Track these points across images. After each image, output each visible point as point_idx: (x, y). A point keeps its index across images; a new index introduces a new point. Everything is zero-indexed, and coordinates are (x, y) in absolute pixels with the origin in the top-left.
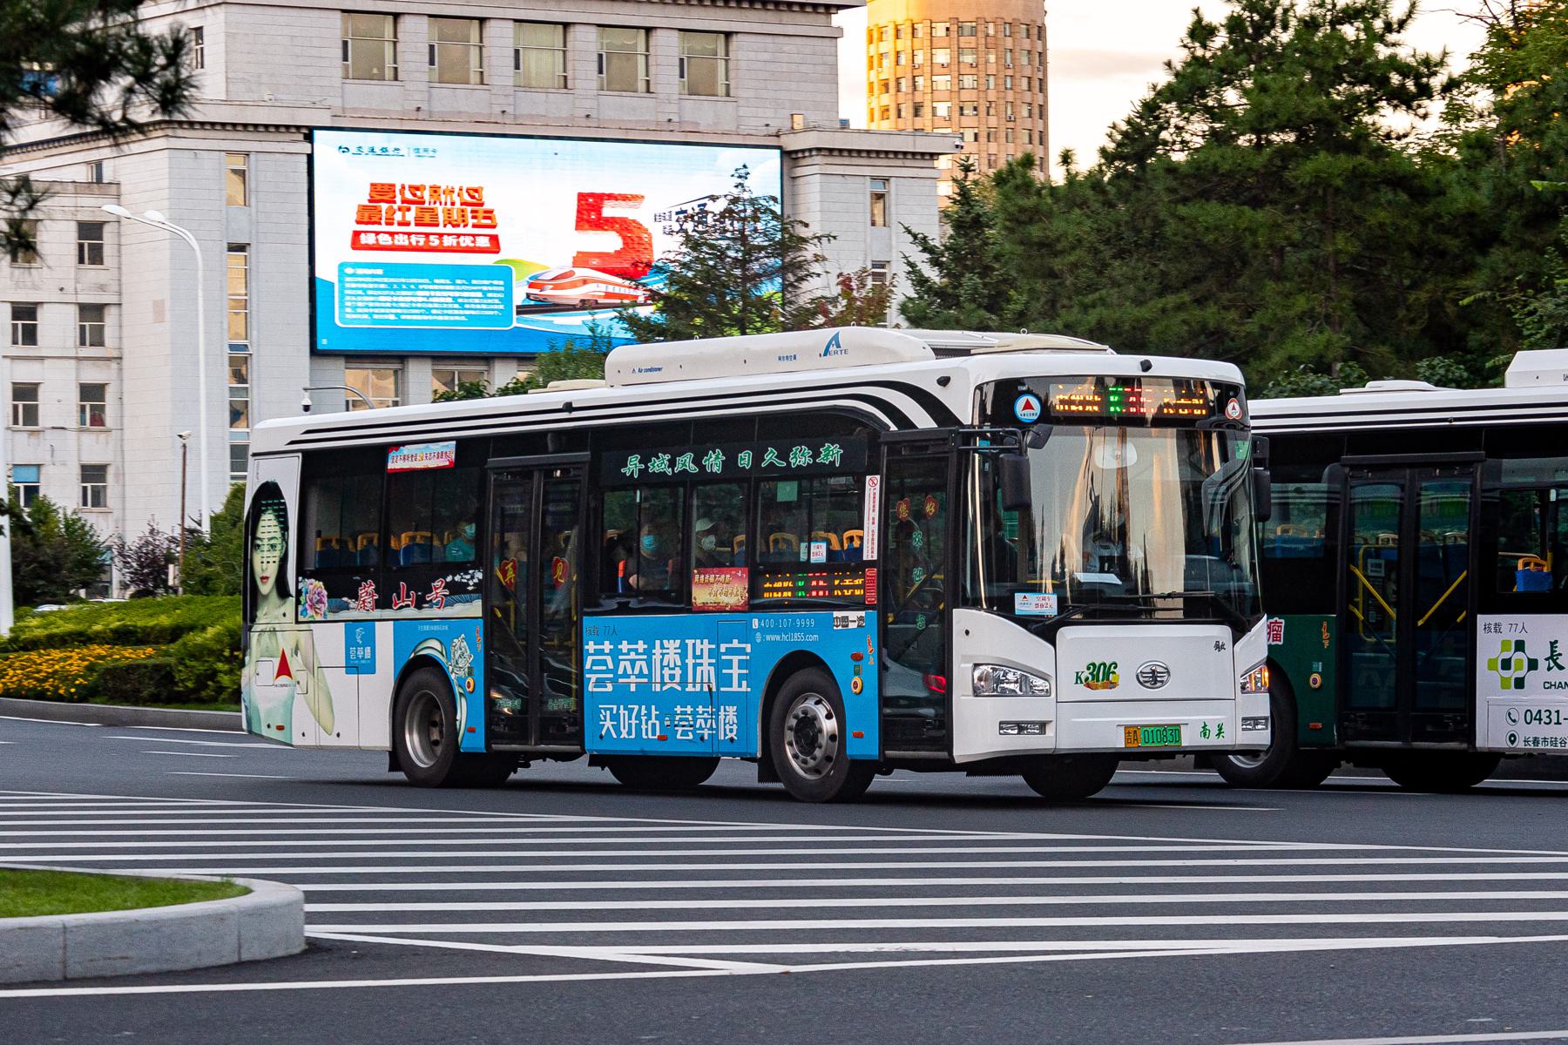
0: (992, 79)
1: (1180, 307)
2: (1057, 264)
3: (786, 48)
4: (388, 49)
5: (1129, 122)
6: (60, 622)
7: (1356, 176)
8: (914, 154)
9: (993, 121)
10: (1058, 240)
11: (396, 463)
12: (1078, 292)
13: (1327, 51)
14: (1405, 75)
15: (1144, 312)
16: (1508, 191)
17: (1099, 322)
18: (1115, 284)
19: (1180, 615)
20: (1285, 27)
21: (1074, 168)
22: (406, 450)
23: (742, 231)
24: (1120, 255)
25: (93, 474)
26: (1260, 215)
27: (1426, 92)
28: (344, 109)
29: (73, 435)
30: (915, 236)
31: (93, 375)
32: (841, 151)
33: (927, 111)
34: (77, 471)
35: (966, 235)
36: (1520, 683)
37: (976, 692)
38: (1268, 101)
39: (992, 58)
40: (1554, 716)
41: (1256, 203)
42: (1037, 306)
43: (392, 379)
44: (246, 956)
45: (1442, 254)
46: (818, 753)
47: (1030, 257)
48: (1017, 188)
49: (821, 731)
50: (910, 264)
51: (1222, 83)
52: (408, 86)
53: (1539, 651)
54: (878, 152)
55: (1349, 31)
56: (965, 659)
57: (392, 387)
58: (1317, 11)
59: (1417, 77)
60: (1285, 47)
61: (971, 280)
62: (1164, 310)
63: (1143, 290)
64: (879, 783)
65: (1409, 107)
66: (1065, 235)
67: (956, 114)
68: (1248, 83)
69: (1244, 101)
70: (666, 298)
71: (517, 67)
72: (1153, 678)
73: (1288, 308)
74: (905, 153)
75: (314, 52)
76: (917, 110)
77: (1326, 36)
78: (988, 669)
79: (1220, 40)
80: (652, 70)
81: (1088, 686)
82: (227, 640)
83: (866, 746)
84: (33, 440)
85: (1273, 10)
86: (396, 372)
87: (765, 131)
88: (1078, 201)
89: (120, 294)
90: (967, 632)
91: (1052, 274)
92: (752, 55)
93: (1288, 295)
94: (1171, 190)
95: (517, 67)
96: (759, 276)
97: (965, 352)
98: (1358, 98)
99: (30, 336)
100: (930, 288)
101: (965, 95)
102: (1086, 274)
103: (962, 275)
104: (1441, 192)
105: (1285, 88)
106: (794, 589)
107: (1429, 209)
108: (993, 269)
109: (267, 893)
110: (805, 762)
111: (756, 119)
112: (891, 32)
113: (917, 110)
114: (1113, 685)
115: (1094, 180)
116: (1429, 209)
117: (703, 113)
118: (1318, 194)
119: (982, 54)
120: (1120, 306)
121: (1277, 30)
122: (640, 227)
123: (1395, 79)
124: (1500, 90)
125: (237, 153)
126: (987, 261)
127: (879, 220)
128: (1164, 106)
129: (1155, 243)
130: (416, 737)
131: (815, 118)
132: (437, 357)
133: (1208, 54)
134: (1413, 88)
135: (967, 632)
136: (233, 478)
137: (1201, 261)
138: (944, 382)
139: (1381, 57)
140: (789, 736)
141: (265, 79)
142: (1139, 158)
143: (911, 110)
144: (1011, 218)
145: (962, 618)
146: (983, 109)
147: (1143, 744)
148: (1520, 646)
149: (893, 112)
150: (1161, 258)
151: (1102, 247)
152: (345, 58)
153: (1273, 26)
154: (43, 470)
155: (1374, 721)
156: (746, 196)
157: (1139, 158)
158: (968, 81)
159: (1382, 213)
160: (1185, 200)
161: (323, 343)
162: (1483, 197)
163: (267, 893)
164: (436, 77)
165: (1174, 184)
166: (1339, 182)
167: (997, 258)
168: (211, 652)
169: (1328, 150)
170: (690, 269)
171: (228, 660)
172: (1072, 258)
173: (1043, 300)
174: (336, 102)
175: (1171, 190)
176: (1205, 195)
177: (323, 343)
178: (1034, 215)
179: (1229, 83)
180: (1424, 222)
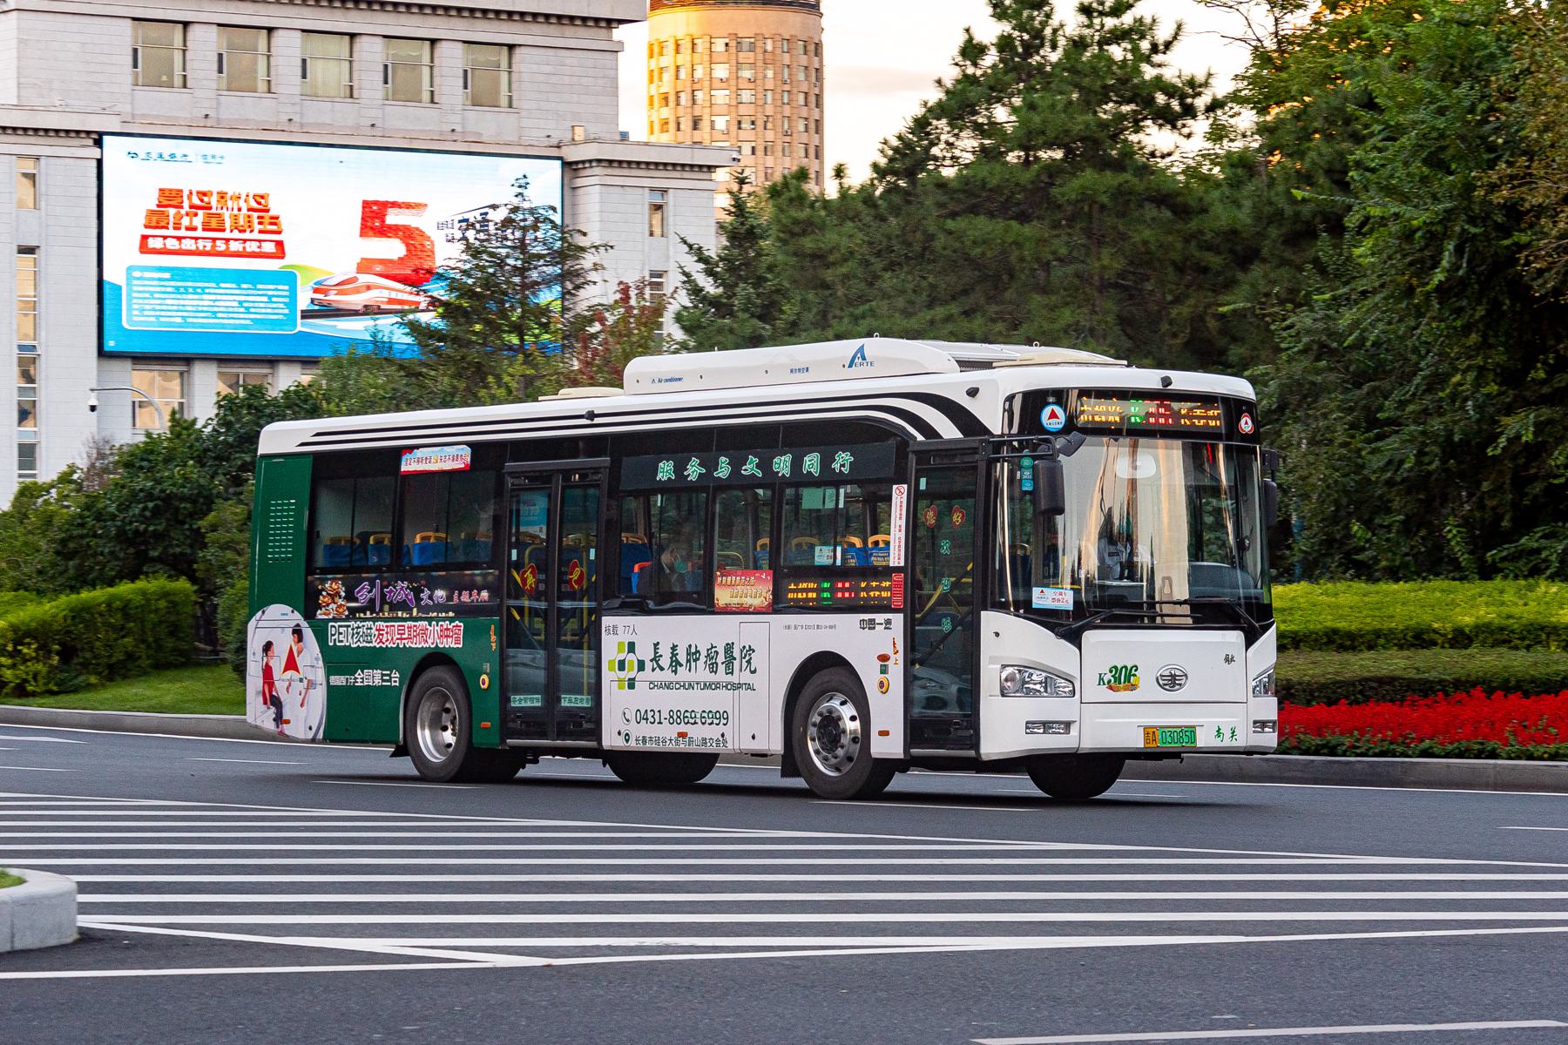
0: (769, 94)
2: (829, 275)
3: (568, 61)
4: (178, 56)
5: (900, 138)
7: (1120, 193)
8: (692, 166)
9: (770, 135)
10: (831, 251)
11: (409, 465)
12: (850, 303)
13: (1095, 71)
14: (1170, 96)
16: (1268, 209)
18: (885, 296)
19: (1189, 621)
20: (1054, 47)
21: (846, 182)
22: (419, 453)
23: (522, 240)
24: (890, 267)
26: (1027, 230)
27: (1189, 111)
30: (690, 247)
32: (620, 162)
33: (705, 124)
35: (740, 246)
38: (1037, 119)
39: (770, 74)
41: (1023, 218)
42: (809, 317)
43: (178, 381)
44: (19, 945)
45: (1205, 270)
46: (840, 752)
47: (802, 268)
48: (791, 200)
49: (844, 732)
50: (685, 274)
51: (990, 101)
52: (198, 93)
54: (657, 164)
55: (1117, 52)
56: (993, 660)
57: (178, 388)
58: (1086, 32)
59: (1182, 97)
60: (1054, 66)
61: (744, 290)
62: (932, 322)
63: (911, 303)
64: (898, 783)
65: (1174, 127)
66: (836, 248)
67: (734, 128)
68: (1017, 101)
69: (1013, 118)
70: (446, 304)
71: (304, 77)
72: (1172, 681)
73: (1053, 321)
74: (683, 165)
76: (696, 124)
77: (1094, 56)
79: (991, 58)
80: (436, 80)
81: (1111, 688)
82: (10, 635)
83: (889, 744)
85: (1042, 30)
86: (182, 374)
87: (547, 142)
88: (851, 214)
90: (997, 634)
91: (825, 286)
92: (535, 68)
94: (941, 205)
95: (304, 77)
96: (538, 283)
97: (987, 365)
98: (1123, 117)
100: (705, 297)
101: (743, 110)
102: (857, 286)
103: (736, 285)
104: (1204, 211)
105: (1053, 106)
106: (868, 589)
108: (766, 280)
109: (41, 884)
110: (826, 759)
111: (538, 128)
112: (671, 47)
113: (696, 124)
114: (1133, 687)
115: (866, 193)
116: (1193, 225)
117: (486, 124)
118: (1084, 212)
121: (1046, 50)
122: (422, 234)
123: (1161, 98)
124: (1262, 111)
126: (761, 271)
127: (657, 231)
128: (935, 122)
129: (924, 255)
130: (427, 732)
131: (595, 129)
132: (222, 360)
133: (979, 73)
134: (1177, 108)
135: (997, 634)
136: (20, 476)
137: (970, 275)
138: (973, 392)
139: (1147, 77)
140: (812, 731)
142: (910, 174)
143: (690, 124)
144: (784, 229)
145: (991, 621)
146: (760, 123)
147: (1161, 744)
148: (632, 647)
149: (672, 126)
151: (873, 260)
152: (135, 66)
153: (1042, 45)
155: (1340, 720)
156: (526, 205)
157: (910, 174)
158: (746, 96)
159: (1147, 230)
160: (954, 215)
161: (110, 345)
162: (1244, 216)
163: (41, 884)
164: (224, 85)
165: (944, 199)
166: (1104, 199)
167: (770, 268)
169: (1094, 167)
170: (470, 276)
171: (11, 655)
172: (844, 270)
173: (815, 310)
175: (941, 205)
176: (973, 210)
178: (807, 227)
179: (999, 100)
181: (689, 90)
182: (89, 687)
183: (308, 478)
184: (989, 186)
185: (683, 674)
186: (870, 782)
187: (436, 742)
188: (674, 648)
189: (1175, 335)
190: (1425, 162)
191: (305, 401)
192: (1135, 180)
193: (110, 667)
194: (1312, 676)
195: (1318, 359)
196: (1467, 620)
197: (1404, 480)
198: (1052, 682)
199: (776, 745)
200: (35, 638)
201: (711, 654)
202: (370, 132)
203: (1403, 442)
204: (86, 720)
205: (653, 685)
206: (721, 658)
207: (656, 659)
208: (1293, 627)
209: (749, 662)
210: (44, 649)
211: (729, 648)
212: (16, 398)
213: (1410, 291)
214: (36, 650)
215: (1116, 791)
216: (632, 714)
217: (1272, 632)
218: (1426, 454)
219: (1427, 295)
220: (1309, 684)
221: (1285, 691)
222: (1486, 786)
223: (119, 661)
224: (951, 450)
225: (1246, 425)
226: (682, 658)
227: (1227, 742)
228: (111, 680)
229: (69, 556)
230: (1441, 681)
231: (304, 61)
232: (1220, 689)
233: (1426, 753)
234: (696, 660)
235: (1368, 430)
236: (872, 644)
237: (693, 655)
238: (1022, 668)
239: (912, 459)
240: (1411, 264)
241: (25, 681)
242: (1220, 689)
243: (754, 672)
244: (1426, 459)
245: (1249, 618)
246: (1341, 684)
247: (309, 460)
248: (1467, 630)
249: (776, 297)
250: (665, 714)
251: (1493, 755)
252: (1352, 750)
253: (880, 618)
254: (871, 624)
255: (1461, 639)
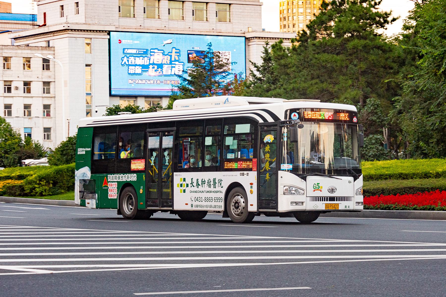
1: (316, 83)
2: (288, 71)
3: (246, 8)
4: (132, 8)
6: (3, 173)
7: (365, 46)
10: (289, 64)
14: (380, 18)
15: (306, 85)
17: (293, 88)
25: (47, 130)
26: (339, 57)
27: (386, 22)
28: (119, 26)
29: (41, 119)
30: (252, 63)
31: (47, 102)
33: (296, 26)
34: (42, 130)
36: (184, 191)
37: (284, 194)
40: (201, 199)
41: (338, 54)
48: (278, 49)
50: (251, 71)
52: (138, 19)
53: (188, 181)
56: (281, 185)
59: (384, 18)
62: (311, 84)
63: (306, 79)
64: (256, 219)
66: (291, 63)
68: (336, 20)
71: (169, 14)
75: (110, 9)
78: (288, 187)
82: (38, 178)
83: (253, 208)
84: (30, 120)
87: (241, 32)
89: (55, 79)
91: (288, 74)
92: (237, 10)
93: (346, 80)
94: (314, 50)
95: (169, 14)
98: (367, 24)
99: (29, 91)
107: (387, 55)
112: (286, 3)
116: (387, 55)
117: (224, 28)
119: (312, 10)
120: (300, 83)
123: (378, 19)
125: (88, 38)
131: (255, 28)
132: (146, 97)
134: (383, 21)
141: (96, 17)
143: (292, 26)
148: (184, 180)
150: (312, 70)
151: (300, 66)
152: (120, 11)
153: (345, 3)
154: (33, 129)
156: (211, 51)
160: (318, 53)
161: (113, 93)
164: (146, 16)
166: (360, 48)
168: (34, 182)
170: (195, 72)
174: (117, 24)
175: (314, 50)
176: (324, 52)
177: (113, 93)
180: (387, 59)
181: (292, 16)
182: (61, 193)
183: (92, 134)
184: (328, 45)
185: (200, 188)
186: (249, 218)
187: (127, 209)
188: (197, 180)
189: (383, 87)
190: (440, 36)
191: (132, 110)
192: (370, 42)
193: (68, 187)
194: (390, 187)
195: (414, 94)
196: (440, 170)
197: (436, 129)
198: (298, 191)
199: (223, 209)
200: (45, 179)
201: (209, 182)
202: (189, 30)
203: (436, 118)
204: (57, 203)
205: (191, 192)
206: (212, 183)
207: (192, 183)
208: (389, 173)
209: (221, 184)
210: (48, 182)
211: (214, 180)
212: (85, 109)
213: (436, 75)
214: (45, 183)
215: (318, 220)
216: (182, 201)
217: (362, 176)
218: (442, 121)
219: (440, 75)
220: (389, 189)
221: (365, 192)
222: (431, 219)
223: (71, 186)
224: (271, 125)
225: (355, 120)
226: (200, 183)
227: (347, 208)
228: (69, 191)
229: (65, 155)
230: (427, 188)
231: (169, 9)
232: (349, 190)
233: (415, 209)
234: (204, 184)
235: (428, 115)
236: (249, 180)
237: (203, 182)
238: (290, 187)
239: (259, 128)
240: (436, 66)
241: (42, 192)
242: (349, 190)
243: (222, 187)
244: (442, 123)
245: (355, 173)
246: (398, 189)
247: (92, 129)
248: (440, 173)
249: (277, 77)
250: (203, 199)
251: (433, 209)
252: (395, 208)
253: (245, 172)
254: (243, 174)
255: (438, 175)
